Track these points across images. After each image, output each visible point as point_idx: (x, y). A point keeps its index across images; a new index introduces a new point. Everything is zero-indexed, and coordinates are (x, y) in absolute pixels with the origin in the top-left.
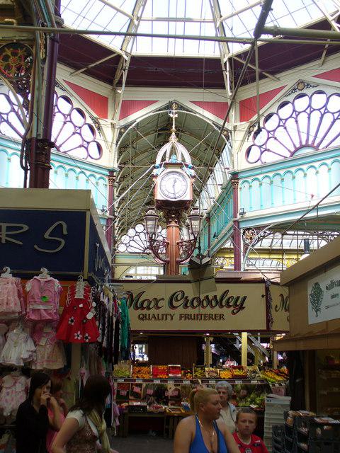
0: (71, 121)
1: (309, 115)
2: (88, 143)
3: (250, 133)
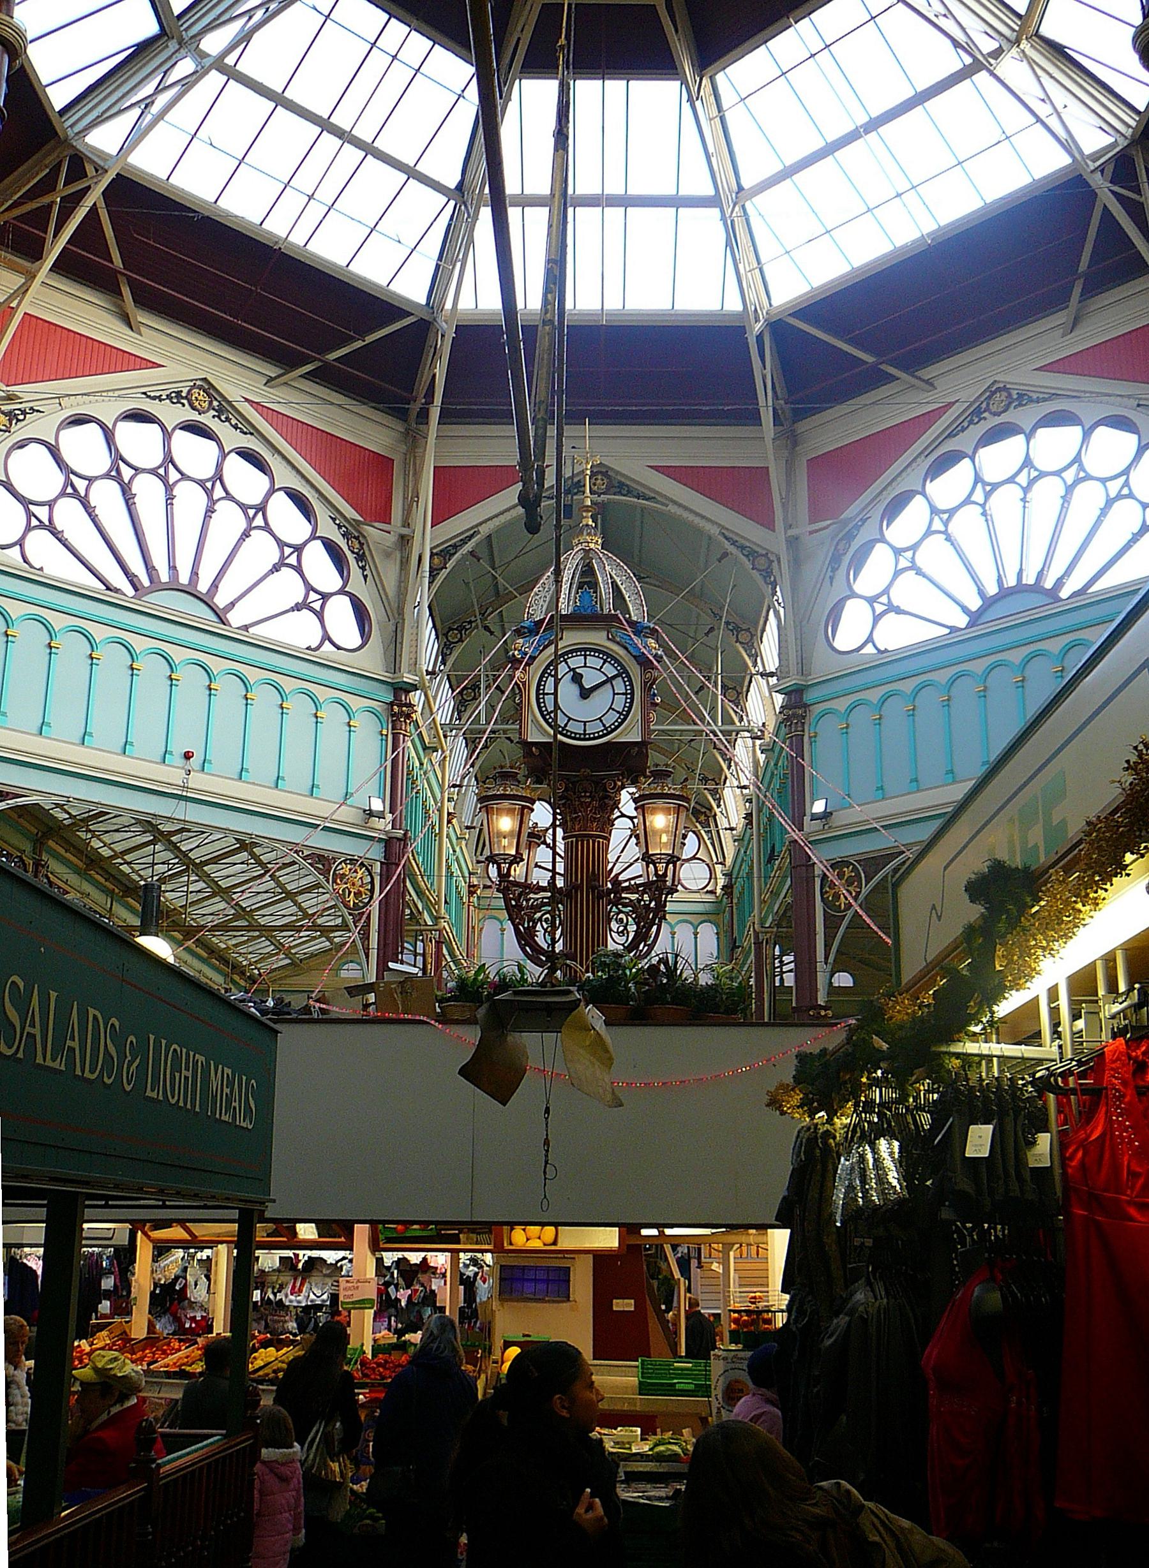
0: (267, 528)
1: (1070, 489)
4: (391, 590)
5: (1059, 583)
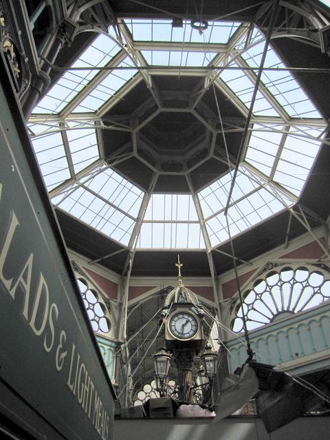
2: (100, 318)
3: (232, 308)
4: (117, 317)
5: (294, 309)
